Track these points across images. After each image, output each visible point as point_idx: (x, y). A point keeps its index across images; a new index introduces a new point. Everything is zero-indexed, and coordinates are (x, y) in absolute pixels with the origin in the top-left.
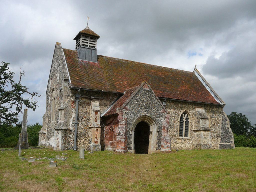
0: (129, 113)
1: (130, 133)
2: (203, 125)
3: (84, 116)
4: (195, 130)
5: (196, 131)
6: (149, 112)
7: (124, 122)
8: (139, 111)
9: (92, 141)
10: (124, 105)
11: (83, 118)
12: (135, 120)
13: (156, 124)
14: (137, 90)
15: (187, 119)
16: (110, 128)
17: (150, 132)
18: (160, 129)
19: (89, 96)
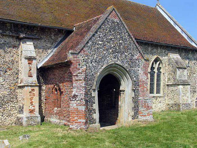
0: (90, 60)
1: (91, 94)
2: (180, 77)
3: (9, 67)
4: (169, 84)
5: (171, 85)
6: (119, 58)
7: (82, 76)
8: (104, 57)
9: (24, 110)
10: (80, 46)
11: (8, 70)
12: (99, 72)
13: (130, 77)
14: (100, 22)
15: (159, 69)
16: (55, 86)
17: (121, 91)
18: (136, 84)
19: (17, 34)
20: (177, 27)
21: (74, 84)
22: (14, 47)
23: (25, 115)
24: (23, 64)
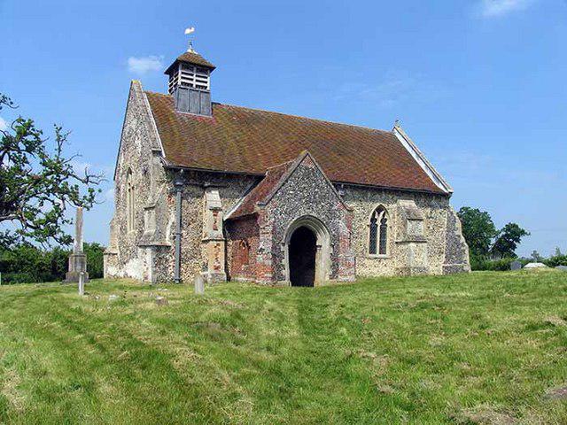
5: (401, 243)
7: (270, 229)
8: (296, 208)
12: (289, 223)
14: (292, 168)
15: (384, 221)
18: (335, 241)
20: (420, 162)
21: (261, 238)
22: (198, 197)
23: (210, 271)
24: (208, 216)
